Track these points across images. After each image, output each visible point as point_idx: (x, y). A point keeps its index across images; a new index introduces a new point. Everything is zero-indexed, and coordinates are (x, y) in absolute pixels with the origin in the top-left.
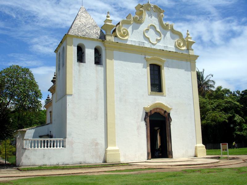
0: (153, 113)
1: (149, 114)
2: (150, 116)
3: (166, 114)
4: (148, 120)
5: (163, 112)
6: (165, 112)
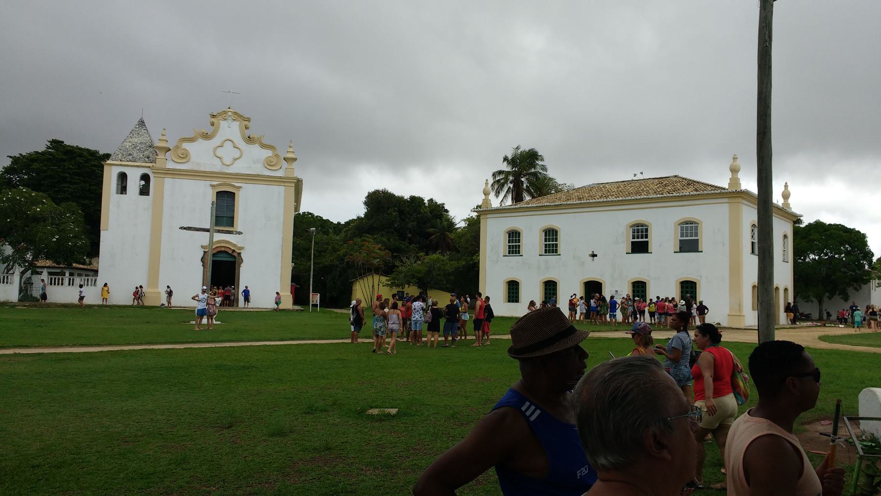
5: (230, 252)
6: (234, 251)
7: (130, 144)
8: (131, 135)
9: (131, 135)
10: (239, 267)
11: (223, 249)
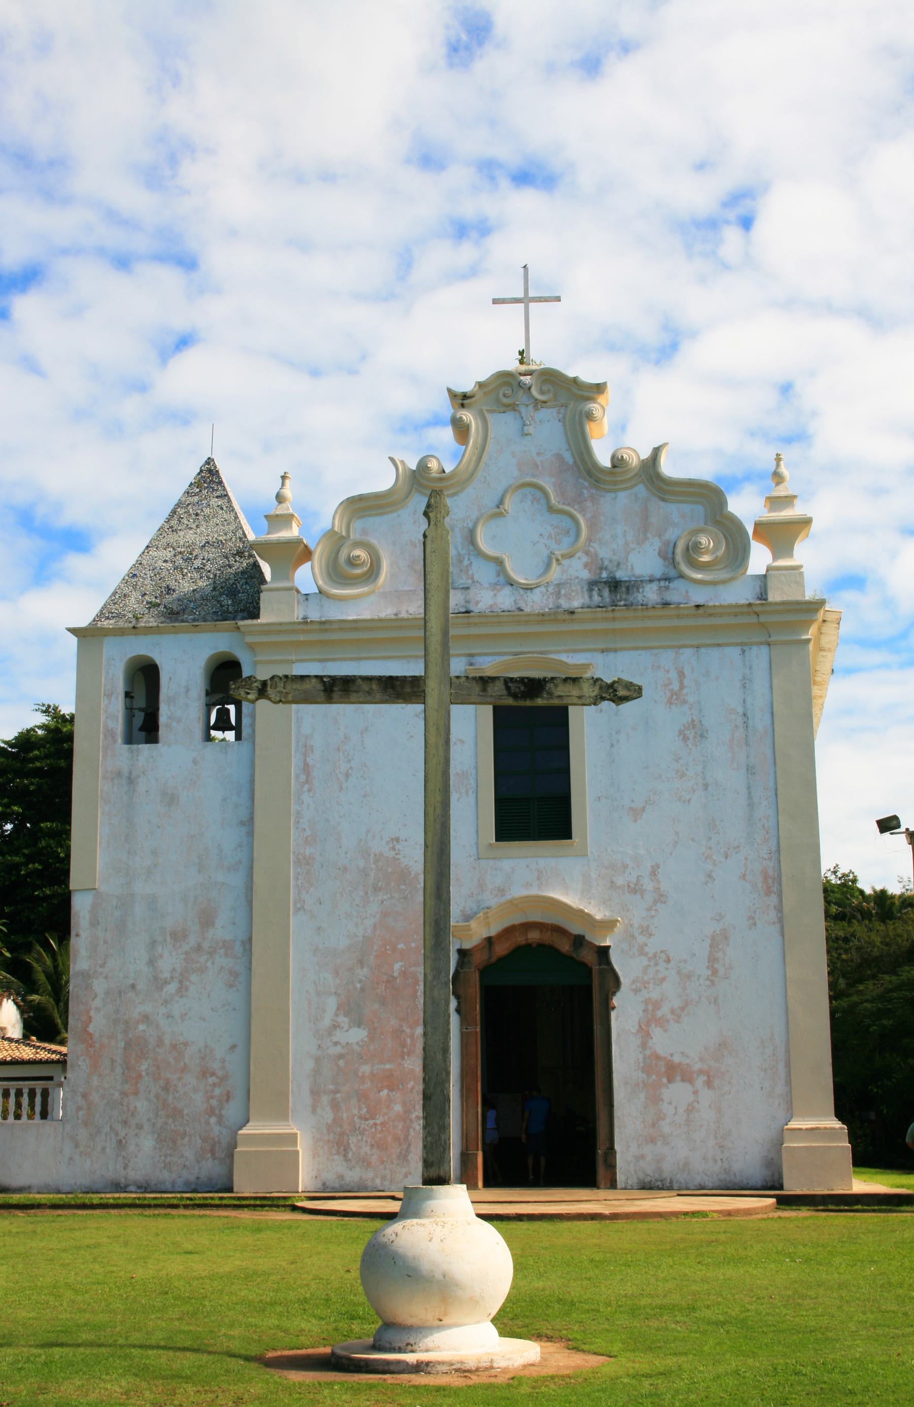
0: (501, 950)
1: (479, 959)
2: (486, 971)
3: (589, 958)
4: (474, 991)
5: (565, 947)
7: (169, 554)
8: (174, 522)
9: (174, 522)
10: (607, 1008)
11: (534, 936)
